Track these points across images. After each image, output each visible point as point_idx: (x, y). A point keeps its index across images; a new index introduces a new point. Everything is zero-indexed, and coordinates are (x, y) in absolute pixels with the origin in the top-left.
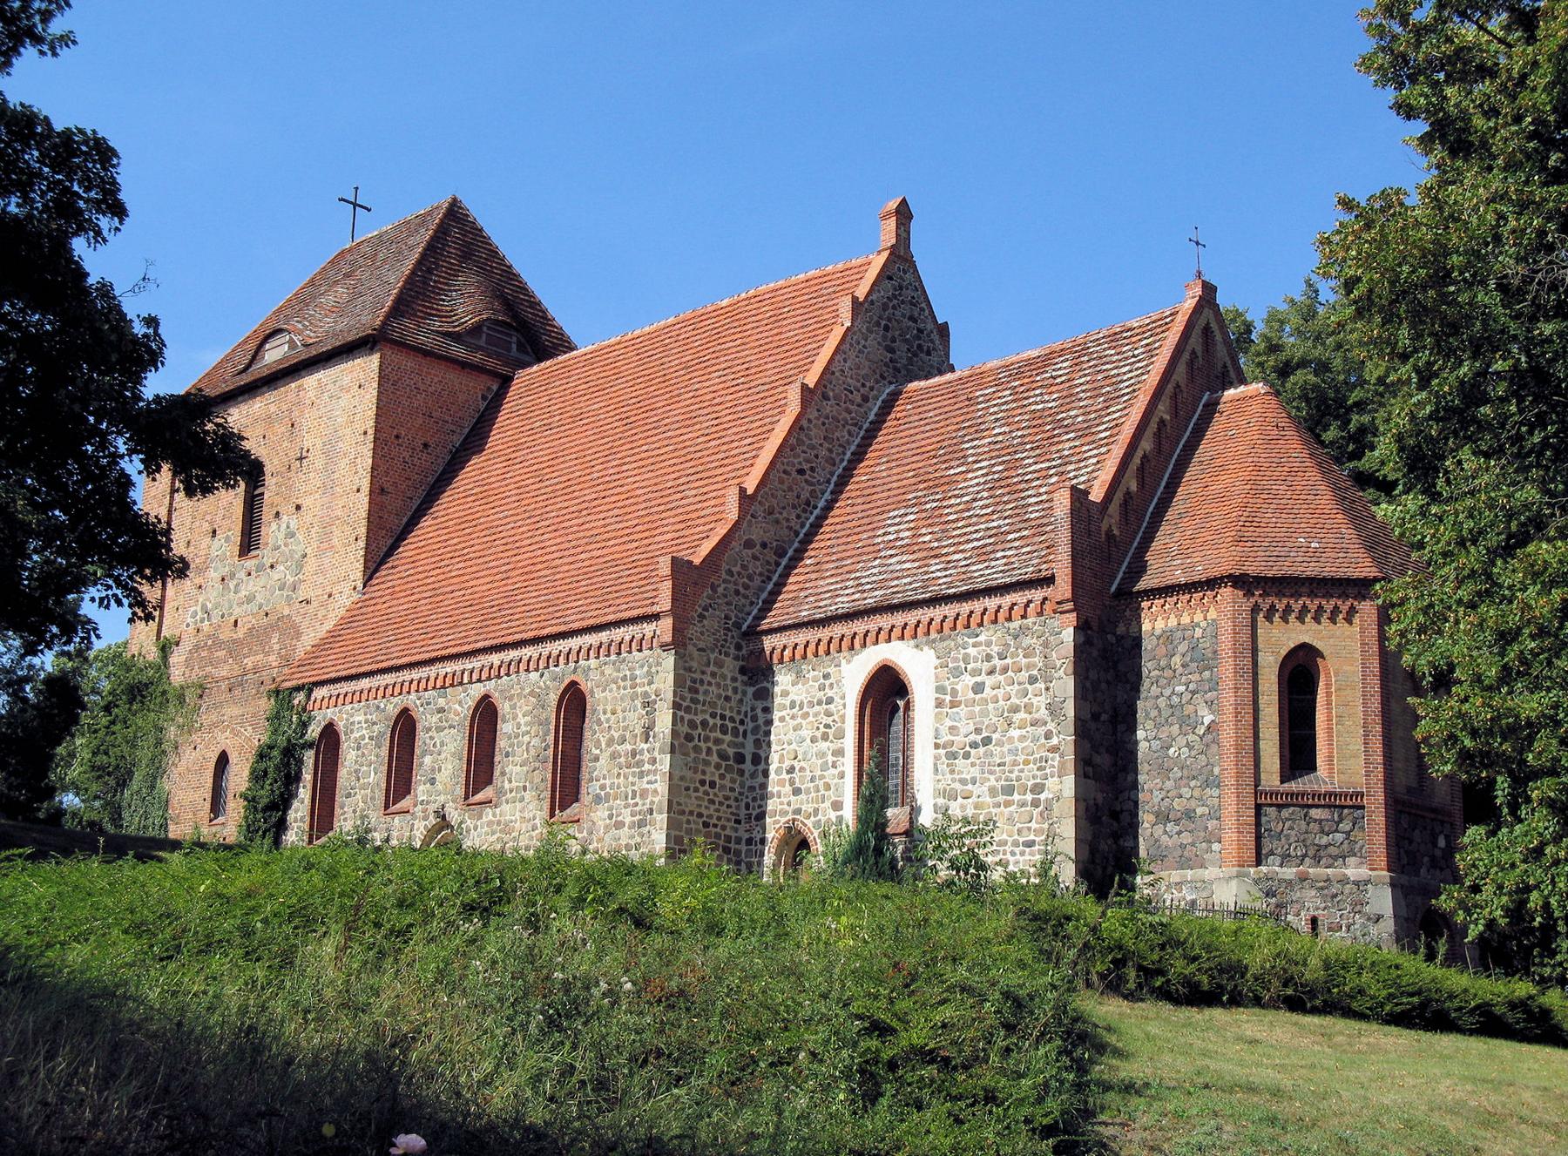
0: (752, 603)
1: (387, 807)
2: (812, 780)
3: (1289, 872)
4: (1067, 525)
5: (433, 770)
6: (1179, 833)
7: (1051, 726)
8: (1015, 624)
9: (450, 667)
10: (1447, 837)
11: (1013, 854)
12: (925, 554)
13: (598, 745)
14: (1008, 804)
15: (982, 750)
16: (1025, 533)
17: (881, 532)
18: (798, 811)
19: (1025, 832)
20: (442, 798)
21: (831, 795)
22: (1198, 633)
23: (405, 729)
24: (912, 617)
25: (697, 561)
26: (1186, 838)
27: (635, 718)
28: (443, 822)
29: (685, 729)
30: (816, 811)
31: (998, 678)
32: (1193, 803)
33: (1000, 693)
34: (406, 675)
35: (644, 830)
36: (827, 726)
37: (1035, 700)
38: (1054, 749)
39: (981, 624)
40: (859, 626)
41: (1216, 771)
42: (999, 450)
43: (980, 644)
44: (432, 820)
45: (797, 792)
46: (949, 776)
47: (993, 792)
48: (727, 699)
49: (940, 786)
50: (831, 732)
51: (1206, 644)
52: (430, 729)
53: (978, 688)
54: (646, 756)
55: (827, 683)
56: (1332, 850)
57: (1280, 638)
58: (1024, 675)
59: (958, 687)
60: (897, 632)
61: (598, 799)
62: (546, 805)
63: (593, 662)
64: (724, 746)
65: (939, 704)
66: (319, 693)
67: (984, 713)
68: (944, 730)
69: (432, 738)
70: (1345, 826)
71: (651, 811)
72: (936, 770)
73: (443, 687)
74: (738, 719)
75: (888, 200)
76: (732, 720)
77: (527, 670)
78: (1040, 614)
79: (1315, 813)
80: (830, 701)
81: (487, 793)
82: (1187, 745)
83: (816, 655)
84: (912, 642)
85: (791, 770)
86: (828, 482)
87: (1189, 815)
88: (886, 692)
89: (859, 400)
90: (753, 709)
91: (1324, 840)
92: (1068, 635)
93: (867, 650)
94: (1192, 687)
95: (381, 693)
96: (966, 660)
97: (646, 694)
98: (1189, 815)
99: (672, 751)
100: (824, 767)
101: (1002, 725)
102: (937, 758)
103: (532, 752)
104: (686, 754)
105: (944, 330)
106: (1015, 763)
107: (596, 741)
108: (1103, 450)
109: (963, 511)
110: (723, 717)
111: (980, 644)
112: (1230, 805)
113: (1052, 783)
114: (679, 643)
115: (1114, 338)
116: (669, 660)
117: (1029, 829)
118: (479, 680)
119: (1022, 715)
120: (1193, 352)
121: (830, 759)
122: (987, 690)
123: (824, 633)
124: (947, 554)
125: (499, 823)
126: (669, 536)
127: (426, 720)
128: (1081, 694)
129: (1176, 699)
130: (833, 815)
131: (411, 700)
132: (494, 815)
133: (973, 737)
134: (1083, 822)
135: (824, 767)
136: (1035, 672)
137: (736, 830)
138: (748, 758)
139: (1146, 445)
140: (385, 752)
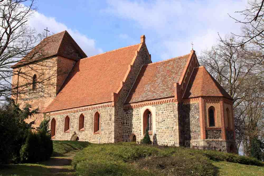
0: (125, 99)
1: (65, 131)
2: (136, 126)
3: (211, 140)
4: (176, 88)
5: (73, 126)
6: (194, 134)
8: (168, 103)
9: (75, 109)
10: (233, 134)
11: (169, 137)
12: (152, 92)
13: (102, 121)
14: (168, 130)
15: (163, 122)
16: (169, 89)
17: (145, 88)
19: (171, 134)
20: (75, 130)
21: (139, 129)
22: (196, 104)
23: (67, 119)
24: (151, 102)
25: (117, 93)
26: (195, 135)
27: (108, 118)
28: (75, 133)
29: (116, 119)
30: (137, 131)
31: (166, 111)
32: (196, 130)
33: (166, 113)
34: (67, 110)
35: (111, 135)
37: (172, 115)
38: (175, 122)
39: (163, 103)
40: (143, 103)
41: (199, 125)
43: (162, 106)
44: (73, 133)
46: (158, 126)
47: (165, 128)
48: (122, 114)
49: (157, 127)
51: (197, 106)
52: (72, 119)
53: (162, 113)
54: (110, 123)
55: (138, 112)
56: (217, 137)
57: (209, 105)
59: (159, 112)
60: (151, 104)
61: (102, 130)
62: (93, 131)
63: (101, 109)
64: (122, 122)
65: (156, 115)
66: (51, 113)
68: (157, 119)
69: (72, 120)
70: (219, 133)
71: (111, 132)
72: (156, 125)
73: (74, 112)
74: (123, 117)
76: (123, 117)
77: (89, 110)
78: (172, 101)
79: (214, 131)
80: (138, 114)
81: (83, 129)
82: (195, 121)
83: (136, 107)
86: (135, 80)
87: (195, 131)
88: (147, 114)
89: (139, 67)
90: (126, 115)
91: (216, 135)
92: (177, 105)
93: (144, 107)
94: (195, 112)
95: (63, 113)
96: (160, 108)
98: (195, 131)
99: (115, 123)
100: (138, 124)
101: (167, 118)
102: (156, 123)
104: (116, 123)
105: (150, 55)
106: (169, 124)
107: (102, 121)
108: (180, 76)
109: (158, 85)
111: (162, 106)
112: (202, 129)
113: (175, 127)
114: (115, 106)
116: (114, 108)
117: (171, 134)
118: (81, 111)
119: (170, 117)
120: (192, 61)
122: (164, 113)
123: (137, 104)
124: (156, 92)
125: (85, 134)
127: (71, 118)
128: (179, 114)
130: (140, 132)
131: (68, 114)
132: (84, 133)
133: (162, 120)
134: (180, 133)
135: (138, 124)
136: (172, 110)
137: (124, 134)
139: (186, 76)
140: (64, 123)
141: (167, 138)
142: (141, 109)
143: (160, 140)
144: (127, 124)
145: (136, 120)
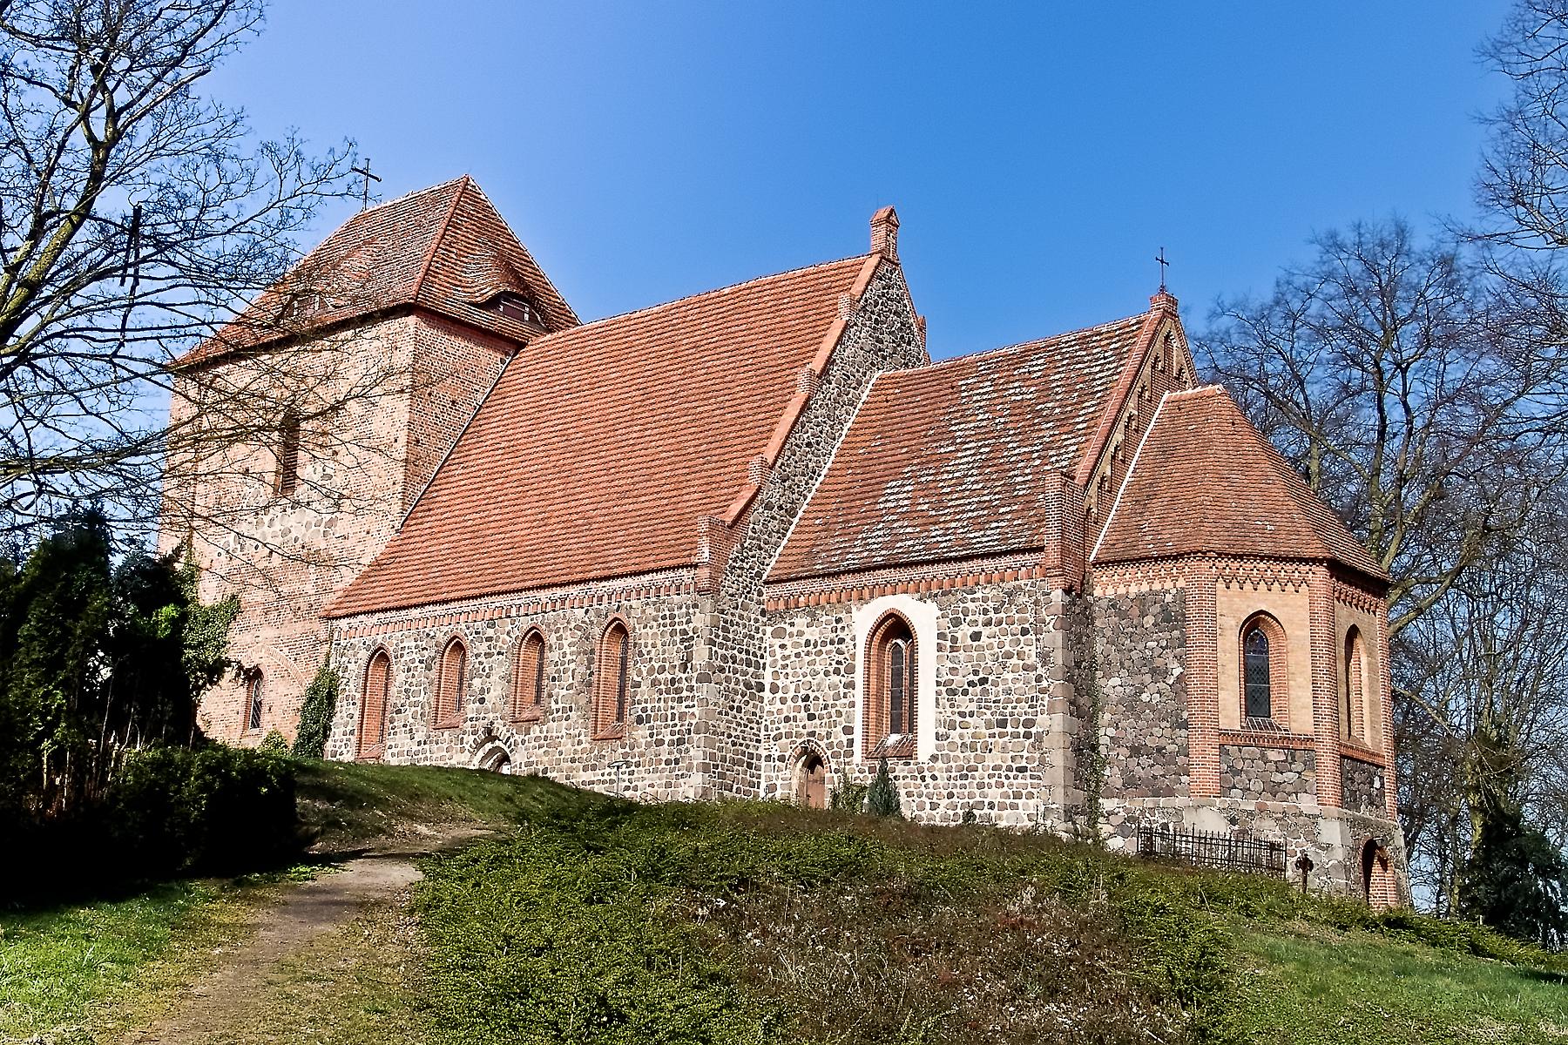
5: (482, 691)
7: (1040, 671)
11: (1007, 777)
13: (639, 673)
14: (1001, 735)
15: (979, 688)
18: (812, 734)
20: (491, 716)
22: (1169, 598)
30: (829, 735)
35: (683, 747)
36: (839, 663)
37: (1026, 649)
40: (867, 578)
41: (1185, 715)
42: (982, 434)
45: (811, 717)
50: (842, 668)
52: (477, 656)
53: (976, 636)
54: (684, 685)
58: (1017, 628)
61: (640, 720)
67: (982, 658)
68: (944, 671)
75: (879, 207)
76: (755, 655)
80: (841, 641)
84: (917, 596)
85: (806, 699)
97: (685, 632)
100: (837, 697)
103: (578, 678)
110: (748, 652)
113: (1042, 720)
115: (1084, 341)
119: (1014, 660)
121: (842, 691)
126: (696, 496)
129: (1148, 653)
130: (844, 738)
133: (971, 677)
135: (837, 697)
138: (767, 687)
141: (993, 781)
142: (854, 609)
143: (955, 786)
144: (780, 694)
145: (827, 674)
